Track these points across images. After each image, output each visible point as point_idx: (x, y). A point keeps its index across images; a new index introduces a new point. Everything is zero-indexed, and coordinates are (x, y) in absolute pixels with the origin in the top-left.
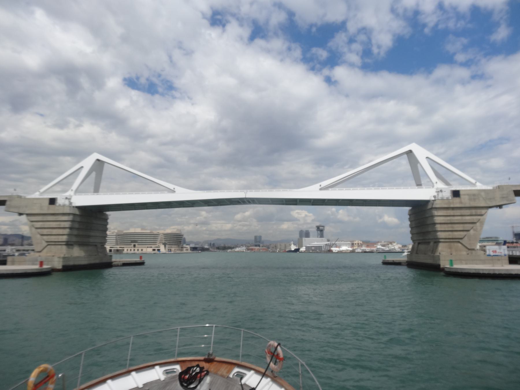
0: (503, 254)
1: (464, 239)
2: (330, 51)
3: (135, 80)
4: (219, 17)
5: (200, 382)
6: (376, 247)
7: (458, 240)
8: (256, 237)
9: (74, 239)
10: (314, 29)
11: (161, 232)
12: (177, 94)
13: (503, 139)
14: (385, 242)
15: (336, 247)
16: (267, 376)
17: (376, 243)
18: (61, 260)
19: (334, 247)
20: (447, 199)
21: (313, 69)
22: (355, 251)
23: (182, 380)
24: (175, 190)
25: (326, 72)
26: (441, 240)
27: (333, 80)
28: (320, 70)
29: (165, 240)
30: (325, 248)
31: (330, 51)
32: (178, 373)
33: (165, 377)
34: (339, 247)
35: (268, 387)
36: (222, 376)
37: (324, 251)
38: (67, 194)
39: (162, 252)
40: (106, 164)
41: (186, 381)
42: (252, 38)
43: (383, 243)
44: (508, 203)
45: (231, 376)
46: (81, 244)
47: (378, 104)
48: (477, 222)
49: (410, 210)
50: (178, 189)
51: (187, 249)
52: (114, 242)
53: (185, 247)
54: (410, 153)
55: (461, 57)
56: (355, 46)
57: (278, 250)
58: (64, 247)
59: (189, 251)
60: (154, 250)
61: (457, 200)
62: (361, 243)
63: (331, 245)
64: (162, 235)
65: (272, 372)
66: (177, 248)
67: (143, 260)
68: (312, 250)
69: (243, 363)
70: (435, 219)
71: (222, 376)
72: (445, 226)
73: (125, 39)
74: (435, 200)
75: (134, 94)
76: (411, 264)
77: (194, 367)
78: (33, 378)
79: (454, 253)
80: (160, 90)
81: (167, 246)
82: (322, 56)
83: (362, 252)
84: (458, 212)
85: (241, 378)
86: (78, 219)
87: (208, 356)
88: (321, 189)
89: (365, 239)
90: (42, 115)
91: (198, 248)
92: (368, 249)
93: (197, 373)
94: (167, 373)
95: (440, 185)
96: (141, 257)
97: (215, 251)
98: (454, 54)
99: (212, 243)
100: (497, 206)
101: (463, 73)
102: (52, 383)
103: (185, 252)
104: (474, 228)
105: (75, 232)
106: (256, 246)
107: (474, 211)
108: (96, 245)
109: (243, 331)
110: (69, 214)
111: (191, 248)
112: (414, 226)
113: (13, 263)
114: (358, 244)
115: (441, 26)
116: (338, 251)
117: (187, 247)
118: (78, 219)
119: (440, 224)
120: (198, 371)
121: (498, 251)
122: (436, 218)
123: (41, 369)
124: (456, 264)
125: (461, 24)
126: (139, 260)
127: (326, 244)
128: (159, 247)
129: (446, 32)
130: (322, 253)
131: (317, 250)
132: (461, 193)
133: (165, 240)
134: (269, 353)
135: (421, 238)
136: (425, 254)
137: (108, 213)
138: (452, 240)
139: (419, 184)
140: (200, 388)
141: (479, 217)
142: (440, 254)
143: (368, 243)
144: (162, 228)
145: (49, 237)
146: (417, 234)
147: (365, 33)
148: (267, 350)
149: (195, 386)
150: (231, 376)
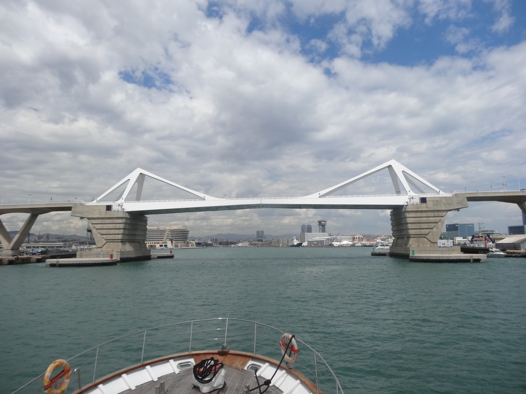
0: (450, 246)
1: (428, 235)
2: (330, 43)
3: (131, 73)
4: (215, 8)
5: (214, 375)
6: (376, 241)
7: (424, 236)
8: (258, 232)
9: (126, 238)
10: (312, 20)
11: (168, 228)
12: (174, 88)
13: (506, 131)
14: (385, 236)
15: (337, 242)
16: (283, 368)
17: (376, 237)
18: (119, 254)
19: (335, 242)
20: (417, 204)
21: (312, 61)
22: (28, 236)
23: (197, 373)
24: (205, 198)
25: (325, 64)
26: (411, 236)
27: (333, 72)
28: (319, 62)
29: (172, 236)
30: (327, 242)
31: (330, 43)
32: (192, 367)
33: (180, 370)
34: (340, 242)
35: (283, 378)
36: (237, 369)
37: (325, 245)
38: (120, 201)
39: (169, 247)
40: (146, 176)
41: (200, 374)
42: (250, 29)
43: (383, 237)
44: (462, 207)
45: (246, 368)
46: (131, 241)
47: (378, 96)
48: (439, 222)
49: (391, 212)
50: (207, 197)
51: (192, 244)
52: (147, 238)
53: (191, 243)
54: (390, 167)
55: (462, 48)
56: (355, 38)
57: (281, 244)
58: (120, 244)
59: (195, 246)
60: (161, 246)
61: (424, 205)
62: (362, 238)
63: (332, 239)
64: (168, 231)
65: (287, 364)
66: (184, 244)
67: (172, 253)
68: (314, 244)
69: (258, 356)
70: (407, 220)
71: (237, 369)
72: (415, 225)
73: (119, 32)
74: (407, 205)
75: (130, 87)
76: (392, 255)
77: (208, 360)
78: (48, 373)
79: (421, 246)
80: (158, 83)
81: (174, 242)
82: (321, 48)
83: (362, 246)
84: (424, 214)
85: (256, 371)
86: (128, 222)
87: (222, 349)
88: (320, 197)
89: (367, 233)
90: (36, 110)
91: (202, 244)
92: (368, 243)
93: (212, 366)
94: (181, 366)
95: (412, 194)
96: (171, 252)
97: (218, 247)
98: (456, 45)
99: (214, 239)
100: (455, 210)
101: (465, 64)
102: (67, 378)
103: (191, 247)
104: (437, 226)
105: (127, 232)
106: (259, 241)
107: (436, 214)
108: (139, 242)
109: (256, 323)
110: (122, 218)
111: (196, 243)
112: (394, 224)
113: (81, 256)
114: (359, 238)
115: (442, 17)
116: (339, 245)
117: (193, 243)
118: (128, 222)
119: (411, 223)
120: (213, 364)
121: (446, 243)
122: (408, 219)
123: (56, 364)
124: (416, 254)
125: (462, 14)
126: (109, 259)
127: (328, 239)
128: (167, 243)
129: (447, 22)
130: (324, 247)
131: (319, 244)
132: (427, 199)
133: (172, 236)
134: (283, 345)
135: (399, 234)
136: (401, 246)
137: (146, 216)
138: (419, 236)
139: (398, 192)
140: (215, 381)
141: (440, 218)
142: (410, 246)
143: (369, 238)
144: (162, 223)
145: (108, 236)
146: (397, 230)
147: (365, 24)
148: (282, 342)
149: (210, 379)
150: (246, 368)
